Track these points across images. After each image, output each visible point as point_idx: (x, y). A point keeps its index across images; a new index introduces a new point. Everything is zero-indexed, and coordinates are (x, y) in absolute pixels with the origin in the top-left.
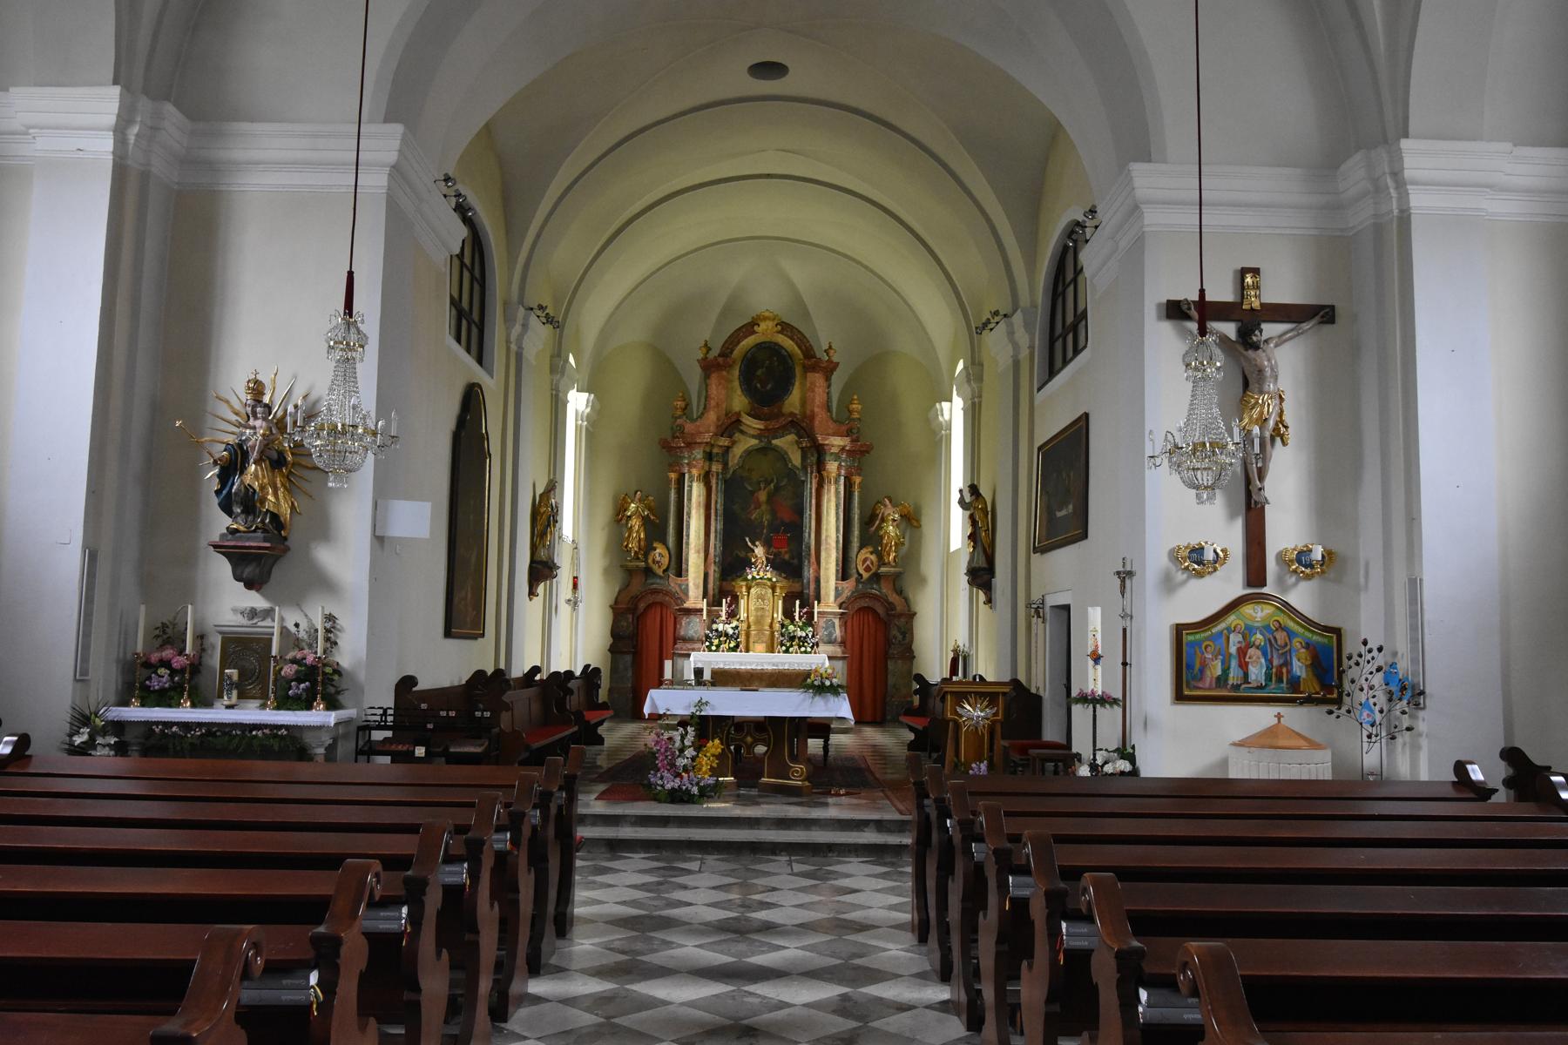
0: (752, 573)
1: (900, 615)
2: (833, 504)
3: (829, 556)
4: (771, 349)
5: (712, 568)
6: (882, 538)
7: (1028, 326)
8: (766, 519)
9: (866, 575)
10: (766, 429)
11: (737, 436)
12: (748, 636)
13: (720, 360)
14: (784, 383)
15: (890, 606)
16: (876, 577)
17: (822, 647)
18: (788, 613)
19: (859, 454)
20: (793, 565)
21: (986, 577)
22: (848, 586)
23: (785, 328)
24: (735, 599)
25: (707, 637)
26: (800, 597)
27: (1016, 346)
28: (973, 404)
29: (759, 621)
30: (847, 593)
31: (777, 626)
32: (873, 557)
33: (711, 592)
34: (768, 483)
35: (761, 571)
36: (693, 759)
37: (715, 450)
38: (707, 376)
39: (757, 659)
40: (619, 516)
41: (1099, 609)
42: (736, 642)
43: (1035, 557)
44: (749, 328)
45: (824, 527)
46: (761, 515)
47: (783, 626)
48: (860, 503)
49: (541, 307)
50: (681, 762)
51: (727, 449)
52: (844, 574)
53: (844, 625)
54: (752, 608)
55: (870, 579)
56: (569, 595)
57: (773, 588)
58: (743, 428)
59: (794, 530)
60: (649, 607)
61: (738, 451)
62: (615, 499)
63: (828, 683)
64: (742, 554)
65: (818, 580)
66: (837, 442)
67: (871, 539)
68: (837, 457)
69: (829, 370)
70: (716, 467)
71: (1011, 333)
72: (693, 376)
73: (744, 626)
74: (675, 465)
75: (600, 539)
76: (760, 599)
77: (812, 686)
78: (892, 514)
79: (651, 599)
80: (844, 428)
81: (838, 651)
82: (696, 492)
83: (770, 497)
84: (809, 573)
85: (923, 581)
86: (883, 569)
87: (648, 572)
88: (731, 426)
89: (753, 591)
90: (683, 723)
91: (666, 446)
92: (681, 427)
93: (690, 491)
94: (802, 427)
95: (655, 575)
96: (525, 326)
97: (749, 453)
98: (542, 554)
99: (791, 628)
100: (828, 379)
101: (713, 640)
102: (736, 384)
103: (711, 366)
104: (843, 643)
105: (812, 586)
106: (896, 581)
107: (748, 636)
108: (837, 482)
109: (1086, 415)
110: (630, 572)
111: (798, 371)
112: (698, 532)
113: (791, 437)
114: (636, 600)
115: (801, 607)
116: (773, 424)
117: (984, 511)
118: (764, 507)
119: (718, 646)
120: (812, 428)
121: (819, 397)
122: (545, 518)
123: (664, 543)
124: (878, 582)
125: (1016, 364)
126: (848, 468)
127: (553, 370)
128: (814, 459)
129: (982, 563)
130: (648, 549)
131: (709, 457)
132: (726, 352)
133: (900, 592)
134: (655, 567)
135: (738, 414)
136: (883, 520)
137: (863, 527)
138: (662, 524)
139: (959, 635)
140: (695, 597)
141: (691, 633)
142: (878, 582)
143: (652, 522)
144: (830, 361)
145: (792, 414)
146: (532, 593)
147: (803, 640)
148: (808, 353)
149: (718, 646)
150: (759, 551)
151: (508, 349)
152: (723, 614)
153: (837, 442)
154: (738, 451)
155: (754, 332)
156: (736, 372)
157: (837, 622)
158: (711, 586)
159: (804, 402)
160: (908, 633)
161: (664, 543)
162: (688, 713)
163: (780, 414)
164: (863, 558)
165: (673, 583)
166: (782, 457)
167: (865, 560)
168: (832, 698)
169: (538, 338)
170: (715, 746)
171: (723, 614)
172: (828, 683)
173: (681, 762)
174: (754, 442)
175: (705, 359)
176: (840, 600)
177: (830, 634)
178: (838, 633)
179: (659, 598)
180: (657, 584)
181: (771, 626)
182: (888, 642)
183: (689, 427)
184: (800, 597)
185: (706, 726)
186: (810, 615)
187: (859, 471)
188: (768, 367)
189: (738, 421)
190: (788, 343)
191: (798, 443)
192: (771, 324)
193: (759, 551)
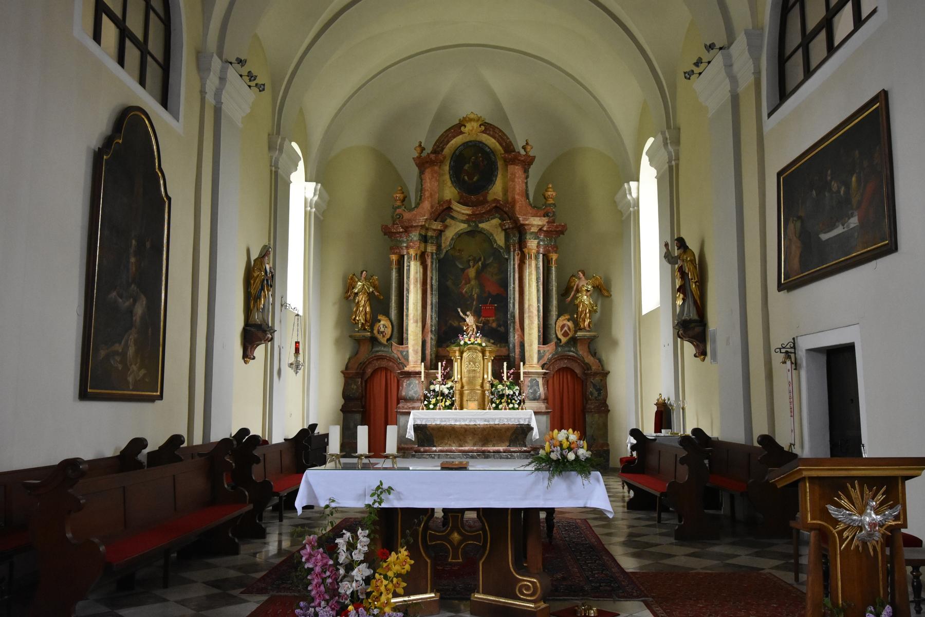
0: (464, 340)
1: (596, 374)
2: (534, 277)
3: (531, 323)
4: (476, 147)
5: (429, 337)
6: (577, 306)
7: (754, 50)
8: (475, 293)
9: (564, 340)
10: (474, 214)
11: (449, 221)
12: (462, 394)
13: (433, 156)
14: (489, 177)
15: (586, 367)
16: (573, 341)
17: (528, 404)
18: (497, 375)
19: (555, 233)
20: (500, 332)
21: (698, 329)
22: (549, 349)
23: (488, 128)
24: (450, 363)
25: (426, 397)
26: (507, 360)
27: (733, 79)
28: (671, 168)
29: (471, 381)
30: (548, 356)
31: (487, 386)
32: (570, 324)
33: (428, 357)
34: (476, 261)
35: (472, 337)
36: (368, 580)
37: (430, 234)
38: (422, 173)
39: (471, 415)
40: (348, 295)
41: (366, 427)
42: (451, 401)
43: (777, 298)
44: (457, 129)
45: (526, 298)
46: (470, 288)
47: (492, 385)
48: (557, 277)
49: (241, 62)
50: (346, 588)
51: (440, 233)
52: (545, 339)
53: (546, 383)
54: (465, 370)
55: (568, 343)
56: (292, 359)
57: (483, 352)
58: (454, 214)
59: (501, 300)
60: (375, 372)
61: (450, 234)
62: (345, 279)
63: (571, 456)
64: (455, 324)
65: (522, 345)
66: (536, 222)
67: (568, 306)
68: (536, 236)
69: (527, 163)
70: (431, 248)
71: (729, 66)
72: (411, 173)
73: (458, 386)
74: (395, 248)
75: (331, 313)
76: (472, 362)
77: (548, 460)
78: (585, 285)
79: (377, 364)
80: (542, 212)
81: (542, 406)
82: (414, 270)
83: (479, 273)
84: (514, 338)
85: (614, 343)
86: (579, 334)
87: (374, 341)
88: (443, 213)
89: (465, 355)
90: (351, 523)
91: (387, 232)
92: (401, 216)
93: (409, 270)
94: (504, 211)
95: (381, 344)
96: (223, 79)
97: (459, 236)
98: (257, 317)
99: (500, 387)
100: (526, 171)
101: (426, 401)
102: (447, 177)
103: (424, 163)
104: (546, 400)
105: (517, 350)
106: (590, 342)
107: (462, 394)
108: (537, 258)
109: (883, 96)
110: (358, 341)
111: (500, 164)
112: (415, 304)
113: (496, 221)
114: (363, 366)
115: (509, 368)
116: (481, 210)
117: (693, 261)
118: (473, 282)
119: (435, 405)
120: (514, 212)
121: (519, 186)
122: (260, 281)
123: (387, 314)
124: (575, 345)
125: (735, 99)
126: (545, 246)
127: (271, 147)
128: (516, 239)
129: (694, 315)
130: (374, 321)
131: (424, 239)
132: (439, 147)
133: (594, 354)
134: (380, 337)
135: (449, 202)
136: (578, 291)
137: (560, 297)
138: (386, 300)
139: (661, 386)
140: (414, 363)
141: (411, 393)
142: (575, 345)
143: (376, 297)
144: (527, 155)
145: (496, 200)
146: (247, 355)
147: (511, 398)
148: (508, 147)
149: (435, 405)
150: (470, 320)
151: (203, 100)
152: (439, 375)
153: (536, 222)
154: (450, 234)
155: (462, 133)
156: (446, 168)
157: (540, 381)
158: (428, 351)
159: (505, 191)
160: (602, 389)
161: (387, 314)
162: (360, 505)
163: (485, 202)
164: (561, 325)
165: (396, 350)
166: (488, 238)
167: (563, 326)
168: (578, 480)
169: (239, 101)
170: (400, 560)
171: (439, 375)
172: (571, 456)
173: (346, 588)
174: (463, 226)
175: (419, 157)
176: (542, 362)
177: (535, 392)
178: (541, 390)
179: (384, 364)
180: (381, 351)
181: (482, 386)
182: (585, 398)
183: (407, 215)
184: (507, 360)
185: (390, 526)
186: (517, 376)
187: (556, 249)
188: (473, 162)
189: (449, 209)
190: (491, 142)
191: (501, 225)
192: (475, 125)
193: (470, 320)
